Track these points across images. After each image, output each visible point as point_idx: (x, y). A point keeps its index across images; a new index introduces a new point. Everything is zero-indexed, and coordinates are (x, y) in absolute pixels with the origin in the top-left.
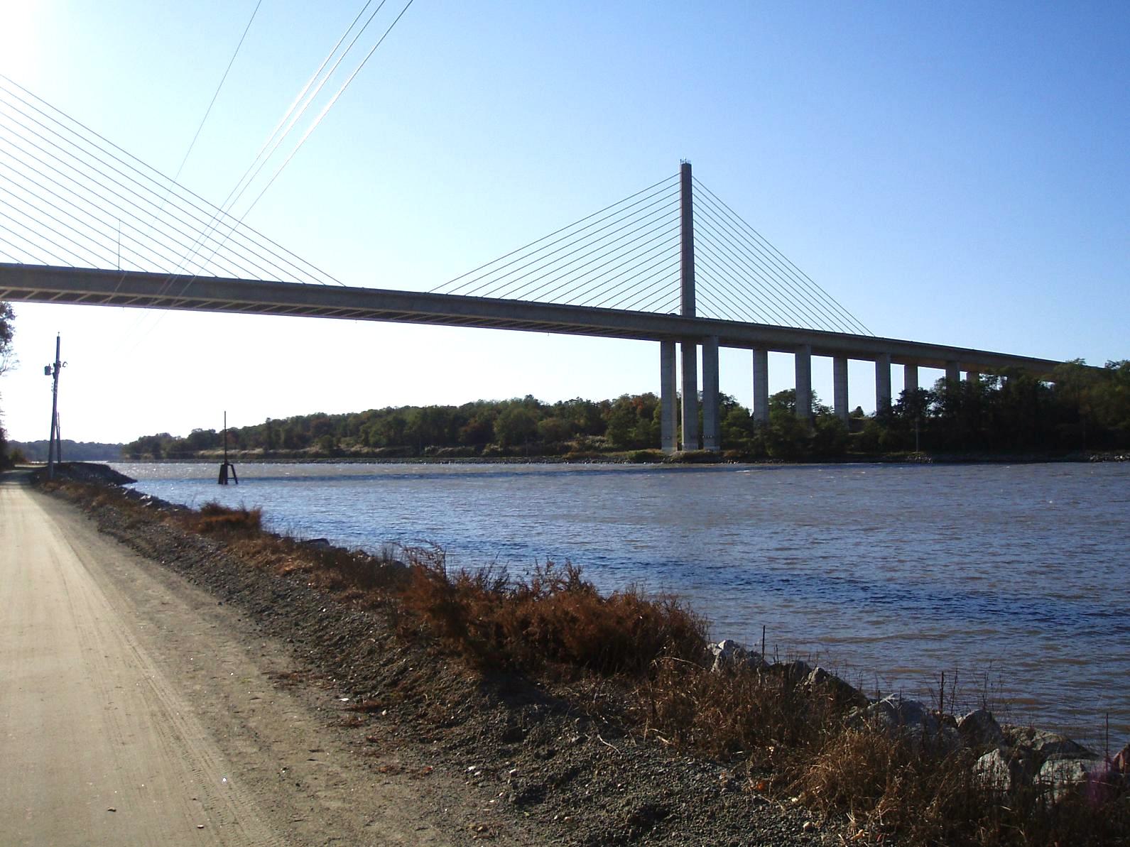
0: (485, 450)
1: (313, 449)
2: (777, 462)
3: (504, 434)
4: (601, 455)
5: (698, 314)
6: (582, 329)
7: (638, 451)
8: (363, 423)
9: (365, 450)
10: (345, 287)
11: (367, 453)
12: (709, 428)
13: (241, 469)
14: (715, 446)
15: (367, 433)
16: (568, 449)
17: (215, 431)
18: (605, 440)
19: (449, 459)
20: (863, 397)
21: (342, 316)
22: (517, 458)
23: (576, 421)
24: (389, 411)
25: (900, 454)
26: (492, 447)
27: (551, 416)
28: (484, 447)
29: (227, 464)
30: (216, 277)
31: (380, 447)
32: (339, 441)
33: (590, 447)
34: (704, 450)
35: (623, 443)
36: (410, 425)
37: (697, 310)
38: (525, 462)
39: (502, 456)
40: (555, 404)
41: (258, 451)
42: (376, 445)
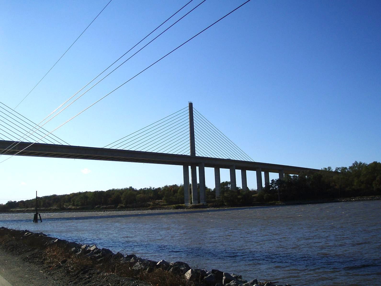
0: (118, 206)
1: (54, 207)
2: (228, 207)
3: (125, 200)
4: (162, 207)
5: (196, 155)
6: (146, 160)
7: (177, 205)
8: (71, 198)
9: (73, 207)
10: (47, 144)
11: (74, 208)
12: (202, 196)
13: (44, 215)
14: (205, 202)
15: (74, 201)
16: (149, 205)
17: (16, 202)
18: (162, 202)
19: (105, 210)
20: (252, 185)
21: (55, 156)
22: (131, 209)
23: (149, 195)
24: (80, 193)
25: (272, 202)
26: (121, 205)
27: (140, 193)
28: (118, 205)
29: (37, 214)
30: (4, 140)
31: (79, 206)
32: (63, 204)
33: (157, 204)
34: (201, 204)
35: (170, 203)
36: (90, 198)
37: (196, 154)
38: (134, 210)
39: (125, 208)
40: (140, 190)
41: (33, 209)
42: (77, 205)
